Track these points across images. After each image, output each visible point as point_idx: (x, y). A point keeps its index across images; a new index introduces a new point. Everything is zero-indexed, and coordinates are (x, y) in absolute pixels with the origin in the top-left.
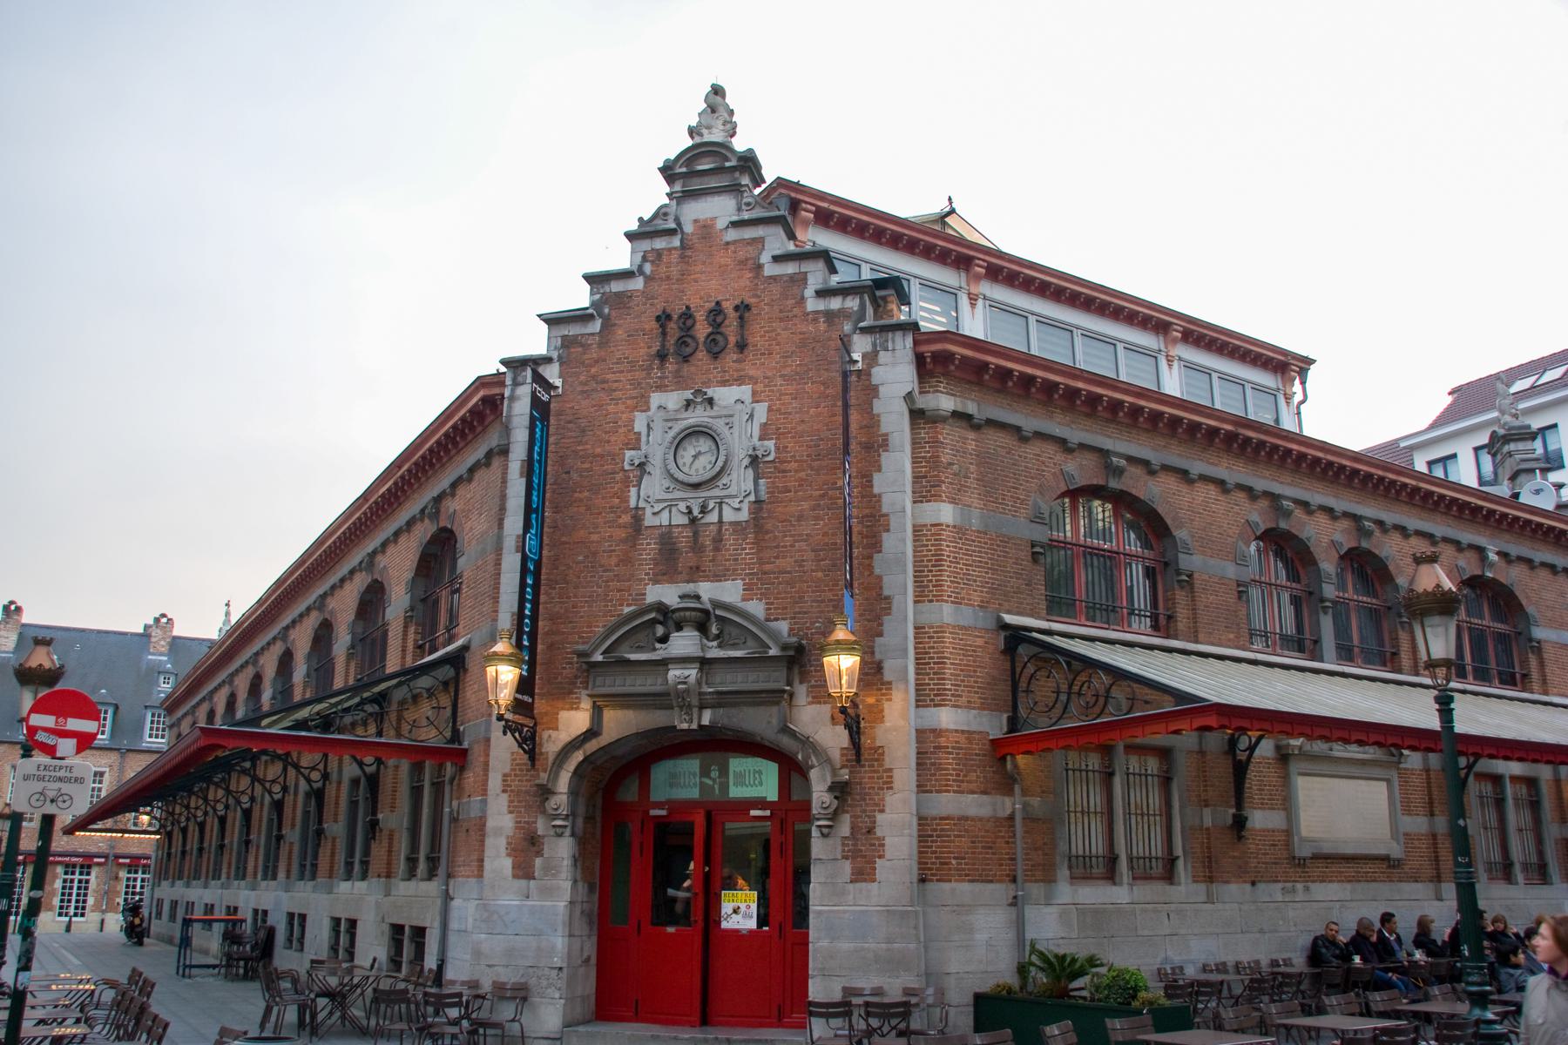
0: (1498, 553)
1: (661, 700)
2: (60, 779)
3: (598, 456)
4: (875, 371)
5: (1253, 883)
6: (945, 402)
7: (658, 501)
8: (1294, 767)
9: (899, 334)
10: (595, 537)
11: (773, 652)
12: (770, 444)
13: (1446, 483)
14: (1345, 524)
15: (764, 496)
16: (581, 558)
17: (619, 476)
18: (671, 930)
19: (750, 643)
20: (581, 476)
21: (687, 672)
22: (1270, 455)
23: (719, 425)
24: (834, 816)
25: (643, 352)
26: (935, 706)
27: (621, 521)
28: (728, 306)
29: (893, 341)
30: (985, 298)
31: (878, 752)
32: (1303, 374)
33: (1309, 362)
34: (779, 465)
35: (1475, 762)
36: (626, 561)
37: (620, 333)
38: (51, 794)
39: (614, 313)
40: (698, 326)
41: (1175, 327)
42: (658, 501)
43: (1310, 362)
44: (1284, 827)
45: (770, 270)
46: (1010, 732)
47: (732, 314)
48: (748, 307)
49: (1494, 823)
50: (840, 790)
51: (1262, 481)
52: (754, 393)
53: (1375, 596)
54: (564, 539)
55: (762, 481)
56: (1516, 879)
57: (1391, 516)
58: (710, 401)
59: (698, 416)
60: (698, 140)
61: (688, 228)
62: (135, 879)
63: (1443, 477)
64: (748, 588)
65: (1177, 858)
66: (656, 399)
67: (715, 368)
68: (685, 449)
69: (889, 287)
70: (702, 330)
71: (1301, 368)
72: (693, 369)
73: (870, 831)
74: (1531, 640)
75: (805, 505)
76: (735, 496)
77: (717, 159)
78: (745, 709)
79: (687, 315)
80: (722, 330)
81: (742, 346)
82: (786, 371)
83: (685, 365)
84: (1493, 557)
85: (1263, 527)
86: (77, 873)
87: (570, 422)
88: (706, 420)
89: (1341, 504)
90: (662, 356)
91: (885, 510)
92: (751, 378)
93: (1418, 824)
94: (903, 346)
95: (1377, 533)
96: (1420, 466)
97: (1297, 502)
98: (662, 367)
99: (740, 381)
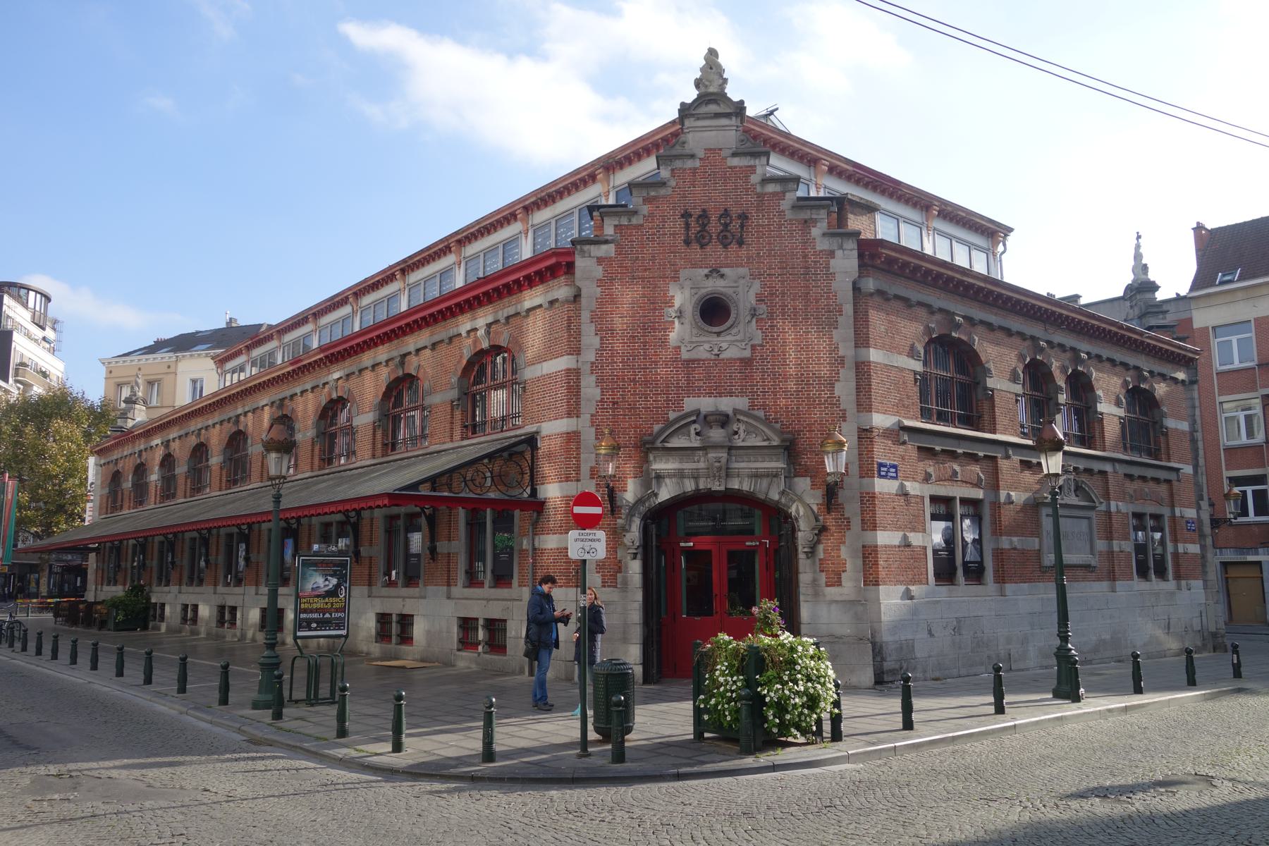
0: (963, 317)
2: (591, 540)
21: (721, 455)
22: (1111, 338)
30: (825, 187)
33: (1011, 230)
38: (587, 549)
41: (824, 162)
43: (1011, 230)
48: (747, 218)
51: (1132, 360)
53: (1147, 416)
56: (1168, 577)
60: (703, 90)
69: (841, 205)
70: (714, 227)
76: (742, 341)
79: (704, 215)
81: (741, 243)
94: (851, 245)
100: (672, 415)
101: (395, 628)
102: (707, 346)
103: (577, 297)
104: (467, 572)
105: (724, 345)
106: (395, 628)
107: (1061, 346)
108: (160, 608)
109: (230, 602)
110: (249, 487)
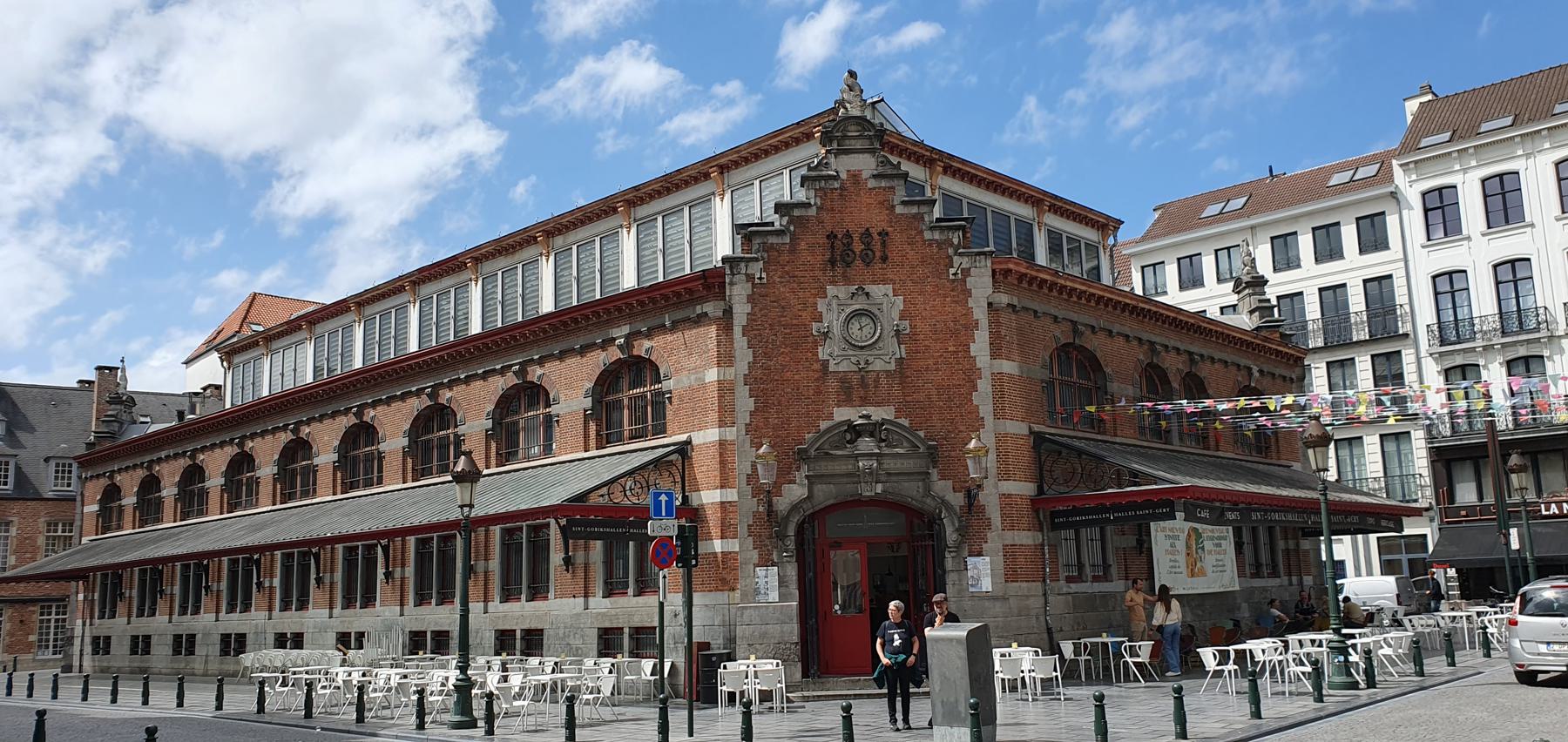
1: (854, 476)
4: (968, 279)
7: (838, 356)
15: (904, 355)
17: (810, 339)
25: (819, 258)
29: (980, 262)
31: (982, 509)
32: (1116, 229)
34: (913, 336)
36: (818, 392)
37: (803, 245)
45: (899, 210)
47: (876, 236)
48: (887, 234)
49: (1098, 537)
52: (894, 290)
55: (902, 346)
58: (867, 294)
61: (843, 176)
62: (49, 620)
64: (898, 410)
66: (831, 290)
67: (868, 272)
71: (1115, 227)
75: (931, 362)
76: (886, 355)
77: (860, 128)
79: (848, 235)
81: (884, 259)
84: (1257, 374)
86: (54, 613)
87: (775, 302)
90: (833, 262)
92: (891, 280)
95: (1088, 332)
98: (833, 269)
99: (884, 282)
100: (824, 425)
102: (854, 359)
103: (728, 312)
105: (871, 359)
108: (356, 639)
109: (103, 633)
110: (314, 501)
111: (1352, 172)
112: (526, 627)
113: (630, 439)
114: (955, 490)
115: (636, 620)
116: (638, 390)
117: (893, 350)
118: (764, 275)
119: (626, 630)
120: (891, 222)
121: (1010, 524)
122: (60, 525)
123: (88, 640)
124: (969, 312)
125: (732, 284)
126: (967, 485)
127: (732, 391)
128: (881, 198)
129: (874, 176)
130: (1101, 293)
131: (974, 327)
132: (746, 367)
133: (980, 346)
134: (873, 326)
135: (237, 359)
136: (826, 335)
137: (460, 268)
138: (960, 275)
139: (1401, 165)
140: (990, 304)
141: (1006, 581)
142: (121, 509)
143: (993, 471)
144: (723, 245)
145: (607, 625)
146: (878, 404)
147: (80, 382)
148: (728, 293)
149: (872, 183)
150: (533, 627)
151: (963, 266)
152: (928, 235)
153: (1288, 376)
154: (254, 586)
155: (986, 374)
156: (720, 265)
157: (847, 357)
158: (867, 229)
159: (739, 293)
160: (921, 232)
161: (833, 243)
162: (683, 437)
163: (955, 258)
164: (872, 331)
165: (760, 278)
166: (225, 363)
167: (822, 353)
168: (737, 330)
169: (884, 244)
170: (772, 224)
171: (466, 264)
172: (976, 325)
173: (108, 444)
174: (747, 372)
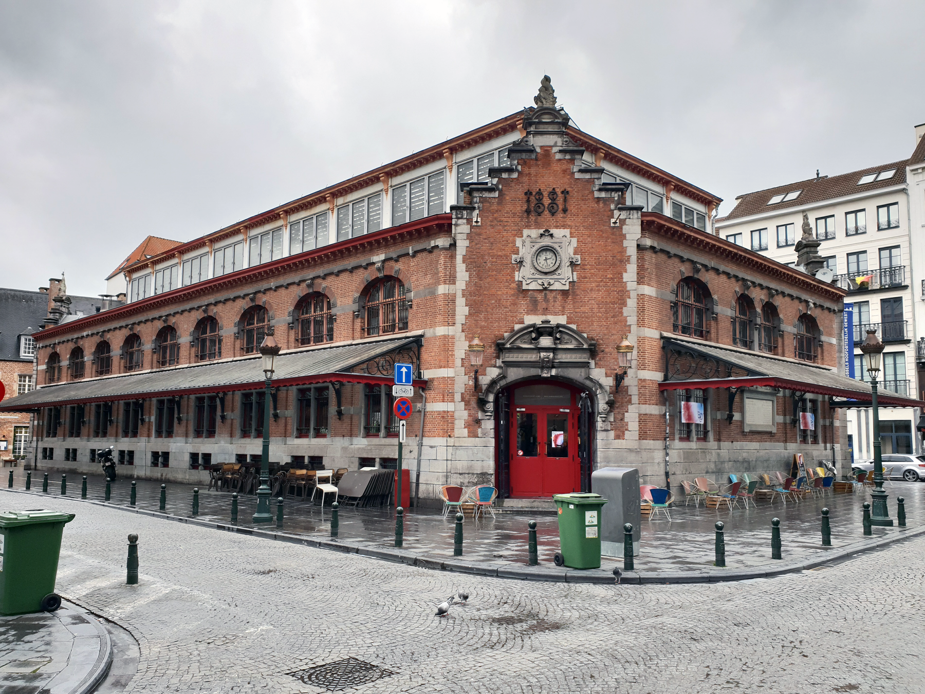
3: (499, 256)
4: (624, 227)
5: (732, 442)
6: (648, 242)
7: (529, 279)
8: (746, 395)
9: (635, 211)
10: (499, 293)
11: (585, 346)
12: (579, 257)
13: (734, 246)
14: (765, 291)
15: (575, 279)
16: (493, 302)
18: (557, 458)
19: (574, 342)
20: (492, 265)
22: (711, 249)
23: (556, 246)
24: (608, 413)
25: (519, 209)
26: (642, 369)
27: (511, 286)
28: (558, 191)
29: (633, 215)
32: (718, 205)
33: (721, 200)
35: (804, 394)
39: (504, 188)
40: (544, 199)
42: (529, 279)
44: (740, 419)
45: (577, 176)
46: (664, 380)
48: (568, 192)
50: (611, 404)
52: (571, 233)
53: (769, 321)
54: (485, 292)
55: (575, 273)
57: (712, 263)
58: (551, 235)
59: (547, 241)
61: (538, 150)
63: (750, 249)
65: (709, 431)
66: (526, 232)
68: (540, 256)
69: (623, 187)
70: (546, 201)
72: (542, 219)
73: (622, 419)
74: (820, 341)
76: (563, 279)
77: (552, 117)
78: (570, 369)
79: (540, 193)
80: (556, 202)
81: (565, 211)
82: (585, 224)
83: (539, 217)
84: (812, 305)
85: (686, 275)
87: (485, 239)
88: (550, 244)
89: (686, 254)
90: (528, 212)
91: (628, 289)
92: (569, 226)
93: (780, 419)
95: (703, 270)
96: (722, 235)
97: (703, 265)
98: (528, 217)
99: (564, 226)
100: (517, 327)
101: (127, 458)
102: (540, 282)
103: (453, 245)
104: (365, 428)
105: (552, 282)
106: (127, 458)
107: (761, 286)
111: (875, 175)
112: (312, 454)
113: (383, 332)
114: (607, 375)
115: (384, 453)
116: (389, 300)
117: (567, 273)
118: (479, 220)
119: (377, 460)
120: (571, 184)
121: (643, 401)
122: (27, 378)
123: (40, 450)
124: (623, 250)
125: (456, 225)
126: (616, 372)
127: (454, 301)
128: (564, 167)
129: (560, 151)
130: (714, 242)
131: (626, 261)
132: (464, 285)
133: (630, 275)
134: (555, 259)
135: (135, 276)
136: (521, 262)
137: (276, 218)
138: (618, 224)
139: (912, 170)
140: (638, 246)
141: (640, 439)
142: (60, 368)
143: (634, 363)
144: (451, 197)
145: (365, 456)
146: (556, 314)
147: (40, 289)
148: (453, 232)
149: (558, 156)
150: (316, 455)
151: (621, 217)
152: (597, 194)
153: (832, 308)
154: (140, 421)
155: (633, 295)
156: (448, 211)
157: (535, 280)
158: (554, 189)
159: (461, 229)
160: (593, 192)
161: (529, 198)
162: (419, 332)
163: (615, 212)
164: (554, 262)
165: (477, 222)
166: (127, 278)
167: (518, 276)
168: (459, 258)
169: (565, 200)
170: (486, 183)
171: (280, 215)
172: (628, 261)
173: (52, 326)
174: (464, 288)
